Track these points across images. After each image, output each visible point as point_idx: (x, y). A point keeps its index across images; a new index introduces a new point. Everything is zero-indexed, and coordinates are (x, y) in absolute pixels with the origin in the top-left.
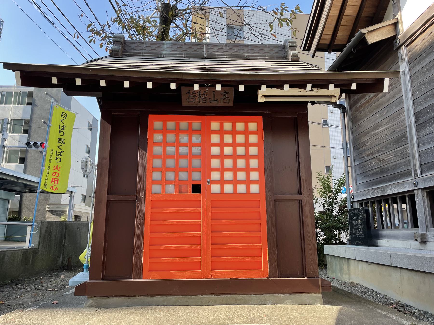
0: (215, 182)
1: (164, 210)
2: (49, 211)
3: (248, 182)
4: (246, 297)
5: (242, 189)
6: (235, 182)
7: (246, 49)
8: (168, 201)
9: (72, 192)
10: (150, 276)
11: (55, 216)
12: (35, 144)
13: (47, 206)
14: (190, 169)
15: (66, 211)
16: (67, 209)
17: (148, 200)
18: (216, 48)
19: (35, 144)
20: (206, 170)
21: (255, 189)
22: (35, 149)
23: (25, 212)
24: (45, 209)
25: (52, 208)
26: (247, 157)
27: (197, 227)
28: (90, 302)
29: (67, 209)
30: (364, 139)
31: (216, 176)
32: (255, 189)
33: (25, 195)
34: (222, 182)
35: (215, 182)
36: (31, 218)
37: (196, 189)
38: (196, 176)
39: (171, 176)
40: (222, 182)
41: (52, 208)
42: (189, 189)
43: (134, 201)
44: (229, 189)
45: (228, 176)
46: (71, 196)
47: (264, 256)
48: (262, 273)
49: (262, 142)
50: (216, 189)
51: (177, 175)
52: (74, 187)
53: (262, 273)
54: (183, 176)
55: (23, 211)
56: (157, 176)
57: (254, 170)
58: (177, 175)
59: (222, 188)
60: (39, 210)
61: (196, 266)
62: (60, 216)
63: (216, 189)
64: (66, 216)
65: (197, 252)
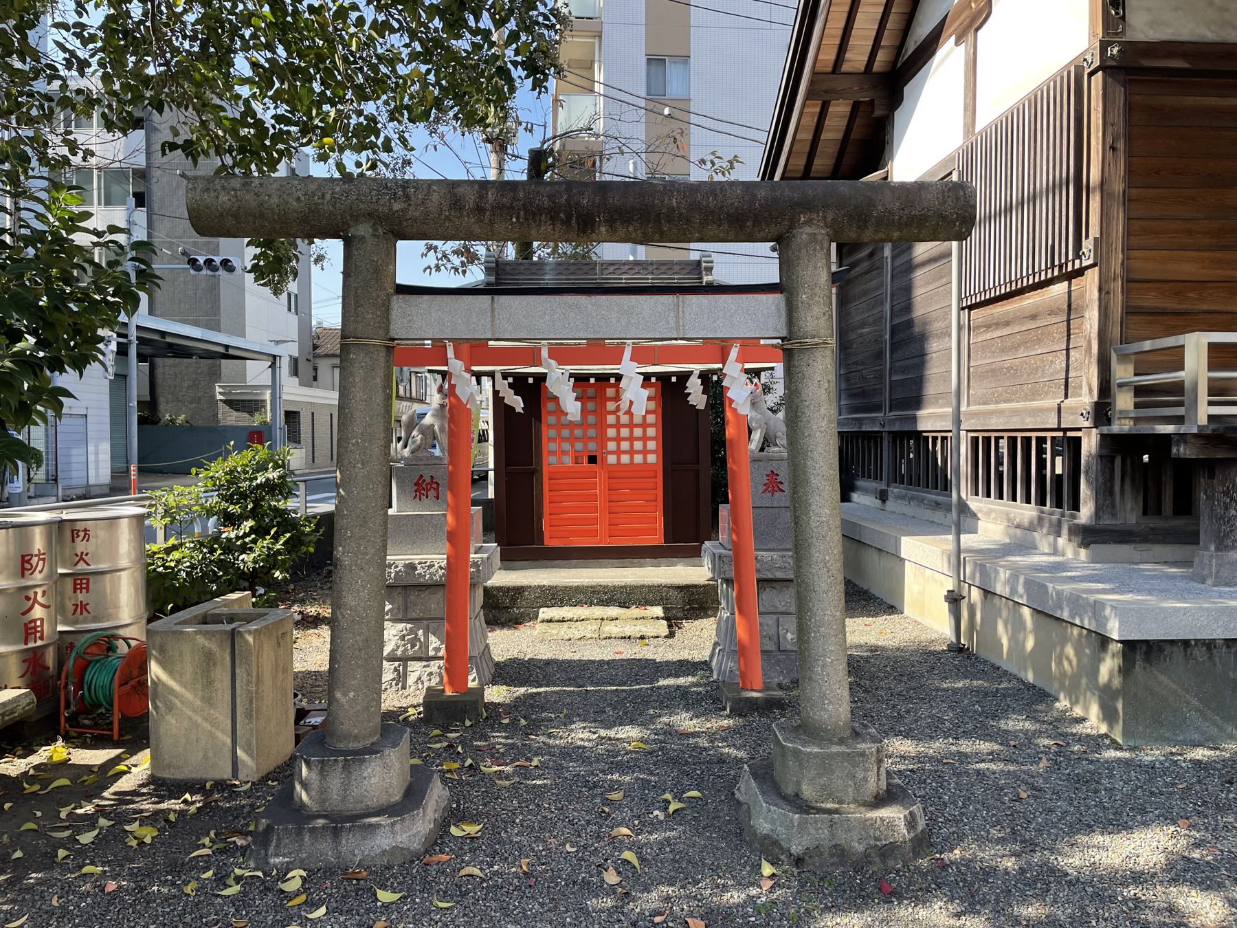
0: (612, 453)
1: (561, 481)
2: (224, 402)
3: (645, 452)
4: (642, 560)
5: (638, 459)
6: (632, 452)
7: (650, 268)
8: (567, 474)
9: (274, 357)
10: (550, 543)
11: (239, 414)
12: (209, 262)
13: (218, 390)
14: (585, 439)
15: (265, 401)
16: (267, 396)
17: (545, 471)
18: (612, 269)
19: (209, 262)
20: (602, 439)
21: (652, 459)
22: (210, 273)
23: (167, 402)
24: (214, 396)
25: (230, 393)
26: (632, 452)
27: (594, 509)
28: (19, 710)
29: (267, 396)
30: (853, 336)
31: (612, 446)
32: (652, 459)
33: (159, 362)
34: (618, 452)
35: (612, 453)
36: (183, 417)
37: (592, 459)
38: (592, 446)
39: (566, 446)
40: (618, 452)
41: (230, 393)
42: (586, 459)
43: (532, 473)
44: (625, 459)
45: (625, 445)
46: (273, 366)
47: (660, 524)
48: (657, 539)
49: (660, 410)
50: (612, 459)
51: (573, 446)
52: (278, 342)
53: (657, 539)
54: (579, 446)
55: (161, 400)
56: (553, 446)
57: (651, 439)
58: (573, 446)
59: (619, 459)
60: (200, 398)
61: (594, 533)
62: (251, 413)
63: (612, 459)
64: (266, 412)
65: (594, 509)
